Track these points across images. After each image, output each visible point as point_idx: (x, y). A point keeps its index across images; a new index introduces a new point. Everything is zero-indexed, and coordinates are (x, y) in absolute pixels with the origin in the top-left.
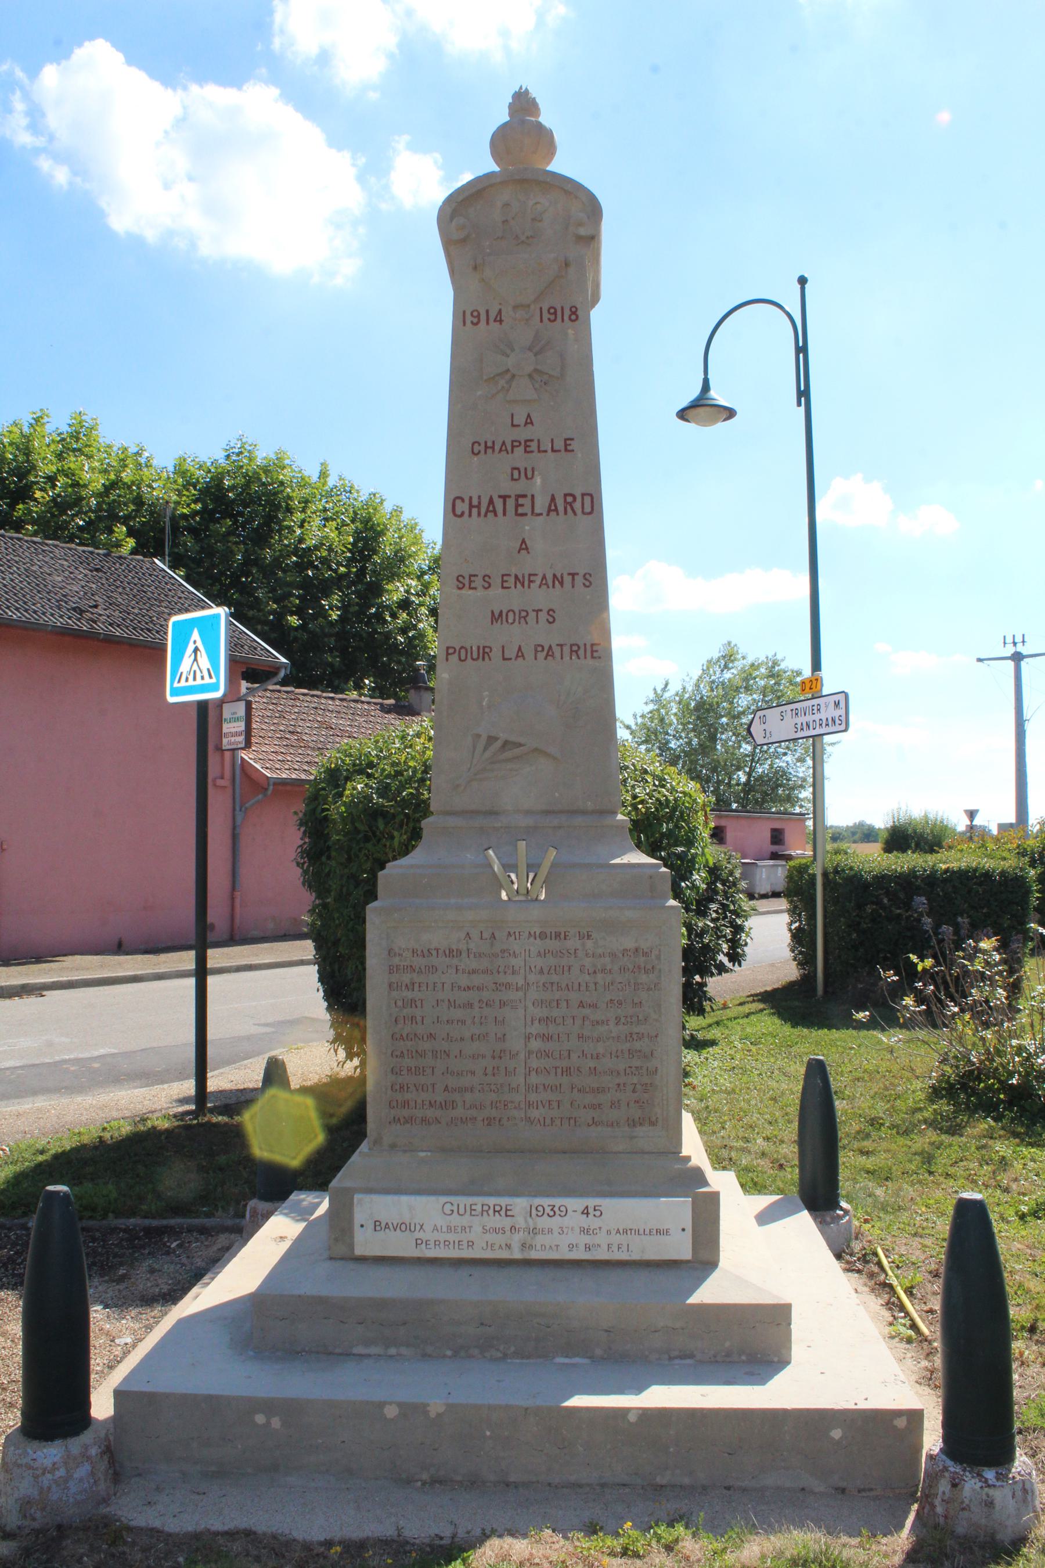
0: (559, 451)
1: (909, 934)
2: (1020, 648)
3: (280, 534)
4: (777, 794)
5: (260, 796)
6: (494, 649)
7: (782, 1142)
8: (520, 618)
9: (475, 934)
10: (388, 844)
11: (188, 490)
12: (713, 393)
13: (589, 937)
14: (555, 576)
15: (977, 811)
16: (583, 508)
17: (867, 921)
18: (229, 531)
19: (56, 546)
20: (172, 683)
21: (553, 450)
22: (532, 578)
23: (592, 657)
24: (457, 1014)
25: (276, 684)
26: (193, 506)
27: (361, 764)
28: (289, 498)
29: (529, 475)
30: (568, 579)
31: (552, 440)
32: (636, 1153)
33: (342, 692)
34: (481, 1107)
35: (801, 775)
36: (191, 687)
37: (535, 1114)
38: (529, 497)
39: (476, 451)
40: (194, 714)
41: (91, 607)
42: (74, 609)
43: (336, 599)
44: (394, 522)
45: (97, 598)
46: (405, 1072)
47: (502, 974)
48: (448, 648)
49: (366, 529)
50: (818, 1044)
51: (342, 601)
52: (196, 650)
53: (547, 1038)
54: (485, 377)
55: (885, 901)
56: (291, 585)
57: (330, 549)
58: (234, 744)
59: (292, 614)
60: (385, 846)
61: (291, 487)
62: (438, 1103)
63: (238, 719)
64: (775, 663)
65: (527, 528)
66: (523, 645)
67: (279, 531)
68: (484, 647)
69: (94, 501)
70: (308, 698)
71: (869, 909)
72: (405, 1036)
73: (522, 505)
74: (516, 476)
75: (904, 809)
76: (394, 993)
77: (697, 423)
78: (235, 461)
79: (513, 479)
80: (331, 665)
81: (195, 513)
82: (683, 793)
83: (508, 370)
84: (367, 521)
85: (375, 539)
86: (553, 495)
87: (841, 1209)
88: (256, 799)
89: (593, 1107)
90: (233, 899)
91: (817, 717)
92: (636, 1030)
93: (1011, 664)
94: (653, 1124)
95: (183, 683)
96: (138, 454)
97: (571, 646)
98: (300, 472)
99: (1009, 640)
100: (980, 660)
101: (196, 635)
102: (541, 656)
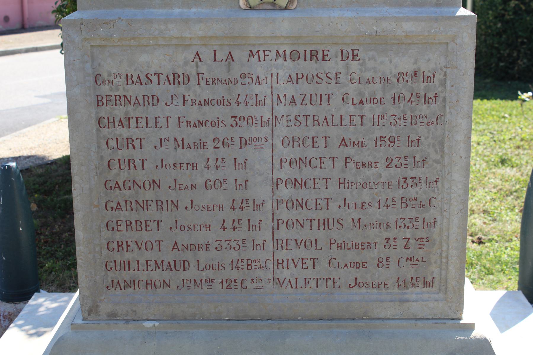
9: (206, 54)
17: (511, 13)
34: (220, 267)
37: (285, 274)
46: (123, 227)
47: (242, 105)
53: (303, 184)
62: (166, 263)
72: (121, 184)
76: (105, 131)
89: (356, 265)
94: (427, 284)
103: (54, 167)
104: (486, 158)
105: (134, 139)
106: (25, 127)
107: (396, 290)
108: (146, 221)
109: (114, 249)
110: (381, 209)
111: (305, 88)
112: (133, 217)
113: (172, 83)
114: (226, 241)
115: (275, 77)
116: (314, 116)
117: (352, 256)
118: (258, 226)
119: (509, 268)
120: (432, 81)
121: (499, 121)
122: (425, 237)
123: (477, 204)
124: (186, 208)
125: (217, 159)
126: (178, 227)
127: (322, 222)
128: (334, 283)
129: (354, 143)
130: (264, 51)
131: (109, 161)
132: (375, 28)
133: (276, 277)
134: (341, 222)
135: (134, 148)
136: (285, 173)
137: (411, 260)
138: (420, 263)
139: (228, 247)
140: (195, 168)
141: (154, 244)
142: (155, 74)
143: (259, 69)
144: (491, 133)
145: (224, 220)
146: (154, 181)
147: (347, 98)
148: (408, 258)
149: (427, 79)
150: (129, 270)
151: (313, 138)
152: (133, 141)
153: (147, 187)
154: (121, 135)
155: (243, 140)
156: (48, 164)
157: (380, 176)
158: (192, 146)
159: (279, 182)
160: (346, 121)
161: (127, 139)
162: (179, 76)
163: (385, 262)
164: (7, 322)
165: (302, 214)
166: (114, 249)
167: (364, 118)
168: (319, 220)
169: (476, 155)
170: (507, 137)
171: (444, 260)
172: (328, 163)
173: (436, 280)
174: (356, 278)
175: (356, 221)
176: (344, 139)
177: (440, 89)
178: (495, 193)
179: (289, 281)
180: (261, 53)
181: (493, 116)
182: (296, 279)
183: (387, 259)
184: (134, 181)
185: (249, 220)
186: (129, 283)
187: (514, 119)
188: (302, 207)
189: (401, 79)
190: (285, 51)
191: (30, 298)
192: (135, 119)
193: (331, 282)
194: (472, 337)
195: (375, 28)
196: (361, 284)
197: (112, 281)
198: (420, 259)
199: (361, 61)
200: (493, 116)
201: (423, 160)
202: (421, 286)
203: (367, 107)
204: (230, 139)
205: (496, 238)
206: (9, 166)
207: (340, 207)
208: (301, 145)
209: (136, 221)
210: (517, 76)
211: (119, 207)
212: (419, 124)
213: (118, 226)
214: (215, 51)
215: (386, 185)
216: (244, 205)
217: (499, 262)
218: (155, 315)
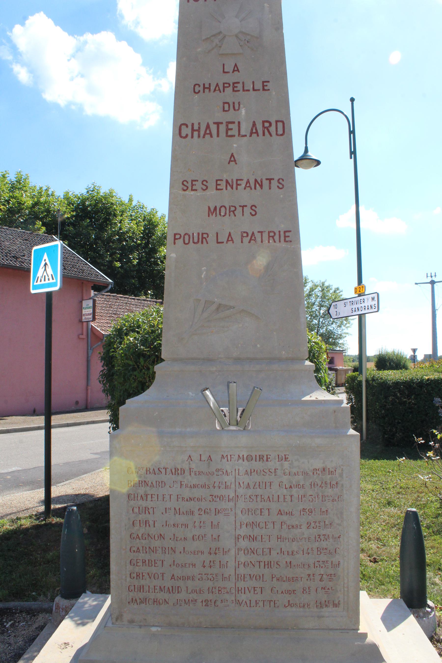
0: (259, 90)
1: (410, 410)
2: (434, 279)
3: (111, 226)
4: (329, 341)
5: (100, 343)
6: (210, 235)
7: (370, 539)
8: (230, 212)
9: (195, 457)
10: (146, 373)
11: (69, 206)
12: (309, 153)
13: (286, 459)
14: (256, 181)
15: (417, 349)
16: (277, 131)
17: (390, 404)
18: (89, 227)
19: (7, 229)
20: (33, 283)
21: (254, 90)
22: (239, 182)
23: (285, 241)
24: (182, 519)
25: (107, 292)
26: (72, 213)
27: (134, 326)
28: (115, 210)
29: (237, 108)
30: (266, 183)
31: (253, 82)
32: (323, 629)
33: (139, 296)
34: (201, 591)
35: (339, 333)
36: (43, 284)
37: (243, 597)
38: (237, 123)
39: (197, 91)
40: (44, 299)
41: (21, 256)
42: (13, 257)
43: (136, 254)
44: (162, 221)
45: (25, 252)
46: (140, 564)
47: (217, 488)
48: (175, 235)
49: (149, 225)
50: (371, 469)
51: (139, 256)
52: (46, 264)
53: (253, 539)
54: (204, 38)
55: (398, 395)
56: (115, 248)
57: (133, 233)
58: (87, 319)
59: (117, 261)
60: (144, 373)
61: (116, 206)
62: (166, 588)
63: (89, 308)
64: (323, 284)
65: (235, 145)
66: (232, 232)
67: (111, 225)
68: (203, 234)
69: (27, 212)
70: (123, 299)
71: (390, 398)
72: (140, 535)
73: (231, 129)
74: (226, 107)
75: (384, 348)
76: (132, 503)
77: (302, 168)
78: (91, 194)
79: (224, 110)
80: (134, 284)
81: (72, 216)
82: (315, 342)
83: (220, 32)
84: (150, 221)
85: (153, 229)
86: (254, 122)
87: (429, 607)
88: (98, 344)
89: (289, 592)
90: (87, 390)
91: (363, 305)
92: (322, 532)
93: (430, 285)
94: (336, 605)
95: (39, 283)
96: (47, 190)
97: (269, 232)
98: (120, 198)
99: (429, 275)
100: (416, 284)
101: (46, 257)
102: (246, 240)
103: (100, 503)
104: (378, 501)
105: (150, 508)
106: (84, 473)
107: (316, 610)
108: (155, 560)
109: (134, 577)
110: (304, 555)
111: (257, 478)
112: (147, 557)
113: (174, 474)
114: (205, 574)
115: (237, 471)
116: (261, 496)
117: (286, 586)
118: (225, 565)
119: (395, 580)
120: (334, 474)
121: (386, 475)
122: (333, 574)
123: (373, 533)
124: (180, 552)
125: (201, 522)
126: (175, 565)
127: (266, 563)
128: (275, 604)
129: (286, 512)
130: (231, 455)
131: (133, 522)
132: (298, 442)
133: (237, 599)
134: (279, 563)
135: (149, 513)
136: (243, 531)
137: (324, 589)
138: (330, 590)
139: (207, 578)
140: (186, 527)
141: (160, 575)
142: (164, 468)
143: (227, 466)
144: (381, 483)
145: (204, 561)
146: (161, 535)
147: (282, 485)
148: (322, 588)
149: (331, 473)
150: (143, 592)
151: (261, 509)
152: (149, 509)
153: (156, 538)
154: (141, 505)
155: (217, 510)
156: (96, 500)
157: (303, 534)
158: (185, 513)
159: (239, 537)
160: (281, 499)
161: (145, 508)
162: (178, 470)
163: (307, 590)
164: (64, 613)
165: (254, 558)
166: (134, 577)
167: (293, 497)
168: (265, 562)
169: (372, 499)
170: (391, 486)
171: (346, 589)
172: (270, 526)
173: (342, 602)
174: (289, 601)
175: (288, 563)
176: (280, 510)
177: (339, 479)
178: (384, 526)
179: (246, 602)
180: (229, 457)
181: (382, 471)
182: (250, 601)
183: (309, 588)
184: (148, 534)
185: (220, 561)
186: (143, 600)
187: (396, 474)
188: (254, 553)
189: (315, 473)
190: (243, 456)
191: (80, 597)
192: (150, 496)
193: (273, 603)
194: (366, 643)
195: (298, 442)
196: (292, 605)
197: (132, 599)
198: (330, 588)
199: (290, 462)
200: (382, 471)
201: (331, 524)
202: (331, 606)
203: (294, 490)
204: (209, 510)
205: (385, 558)
206: (72, 509)
207: (278, 553)
208: (253, 513)
209: (149, 560)
210: (396, 443)
211: (138, 551)
212: (327, 501)
213: (137, 562)
214: (201, 455)
215: (307, 540)
216: (217, 551)
217: (388, 576)
218: (159, 623)
